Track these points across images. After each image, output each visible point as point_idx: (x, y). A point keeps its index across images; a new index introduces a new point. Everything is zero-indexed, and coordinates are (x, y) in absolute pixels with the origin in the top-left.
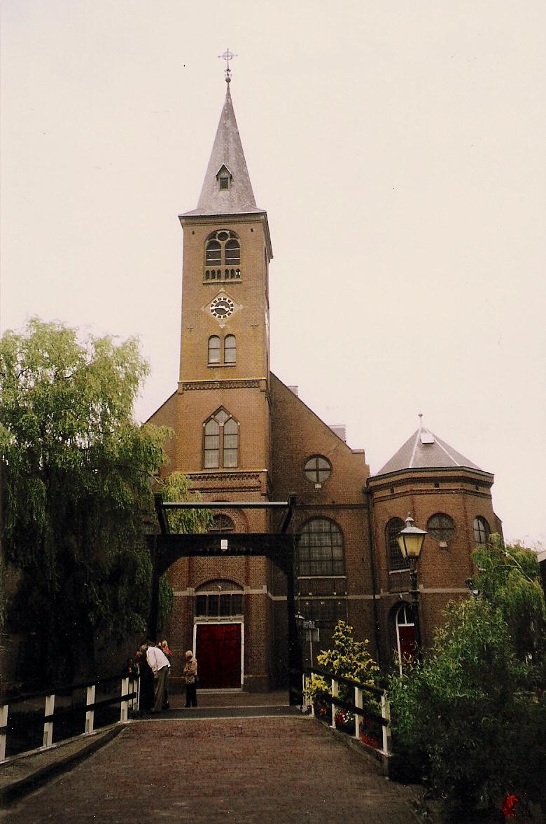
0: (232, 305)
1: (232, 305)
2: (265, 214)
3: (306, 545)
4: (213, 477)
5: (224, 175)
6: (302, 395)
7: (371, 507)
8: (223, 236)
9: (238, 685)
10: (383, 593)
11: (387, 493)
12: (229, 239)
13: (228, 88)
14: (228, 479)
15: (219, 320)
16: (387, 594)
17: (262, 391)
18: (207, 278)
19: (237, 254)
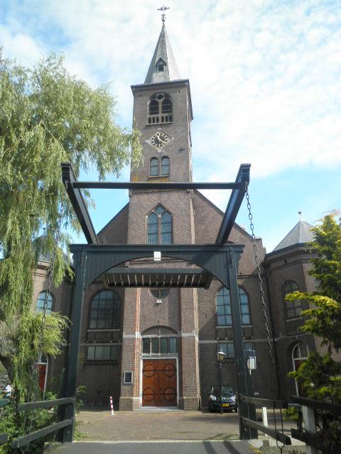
3: (227, 299)
7: (268, 275)
8: (160, 97)
10: (281, 336)
11: (282, 263)
16: (285, 337)
18: (150, 122)
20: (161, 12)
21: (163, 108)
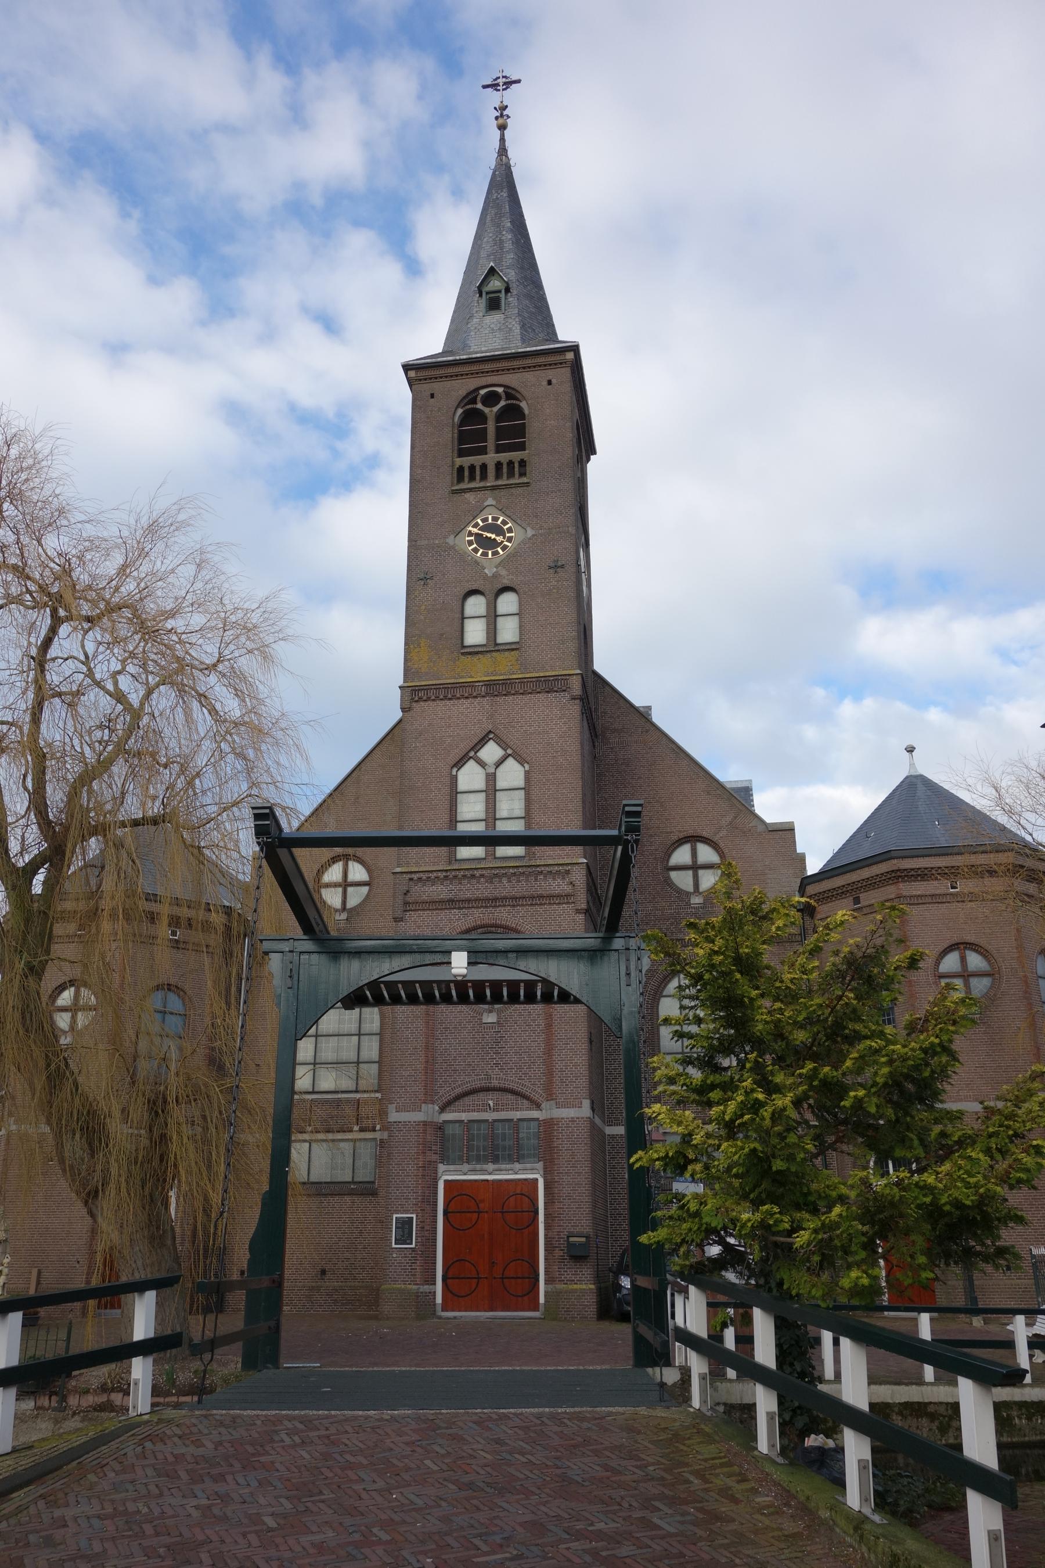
0: (510, 530)
1: (510, 530)
2: (575, 349)
4: (473, 876)
5: (495, 284)
6: (657, 718)
9: (535, 1307)
12: (502, 403)
13: (502, 140)
14: (505, 880)
15: (483, 559)
17: (573, 698)
18: (460, 478)
19: (521, 431)
20: (494, 98)
21: (500, 433)
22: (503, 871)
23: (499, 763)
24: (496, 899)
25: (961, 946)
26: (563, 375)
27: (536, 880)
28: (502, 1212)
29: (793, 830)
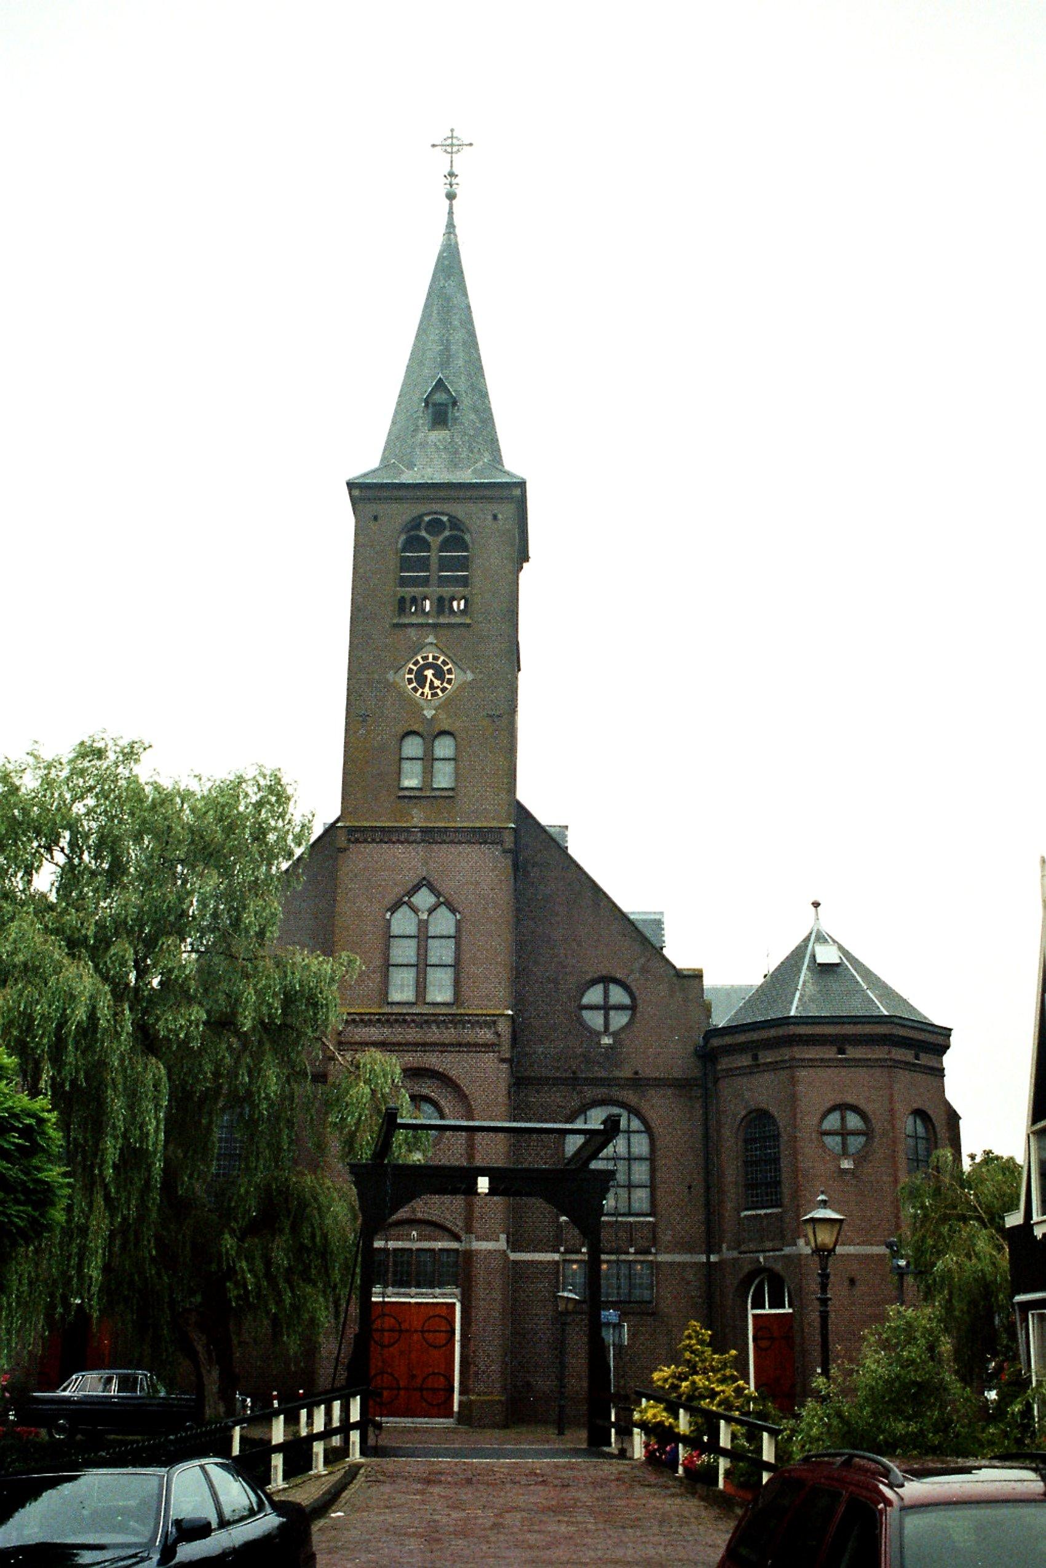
2: (522, 485)
12: (447, 533)
13: (451, 213)
19: (463, 564)
22: (432, 1018)
23: (431, 911)
24: (424, 1044)
25: (843, 1107)
26: (506, 511)
27: (464, 1028)
28: (422, 1332)
29: (702, 976)
